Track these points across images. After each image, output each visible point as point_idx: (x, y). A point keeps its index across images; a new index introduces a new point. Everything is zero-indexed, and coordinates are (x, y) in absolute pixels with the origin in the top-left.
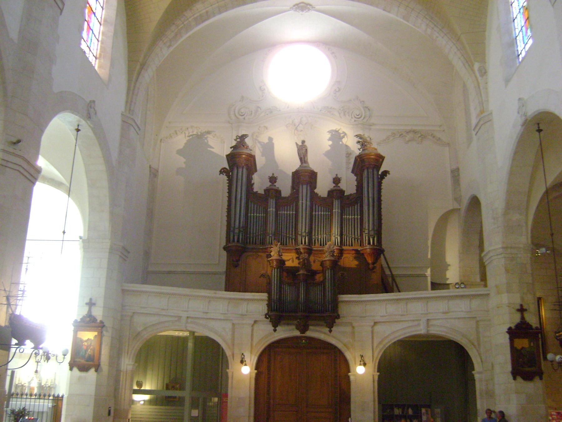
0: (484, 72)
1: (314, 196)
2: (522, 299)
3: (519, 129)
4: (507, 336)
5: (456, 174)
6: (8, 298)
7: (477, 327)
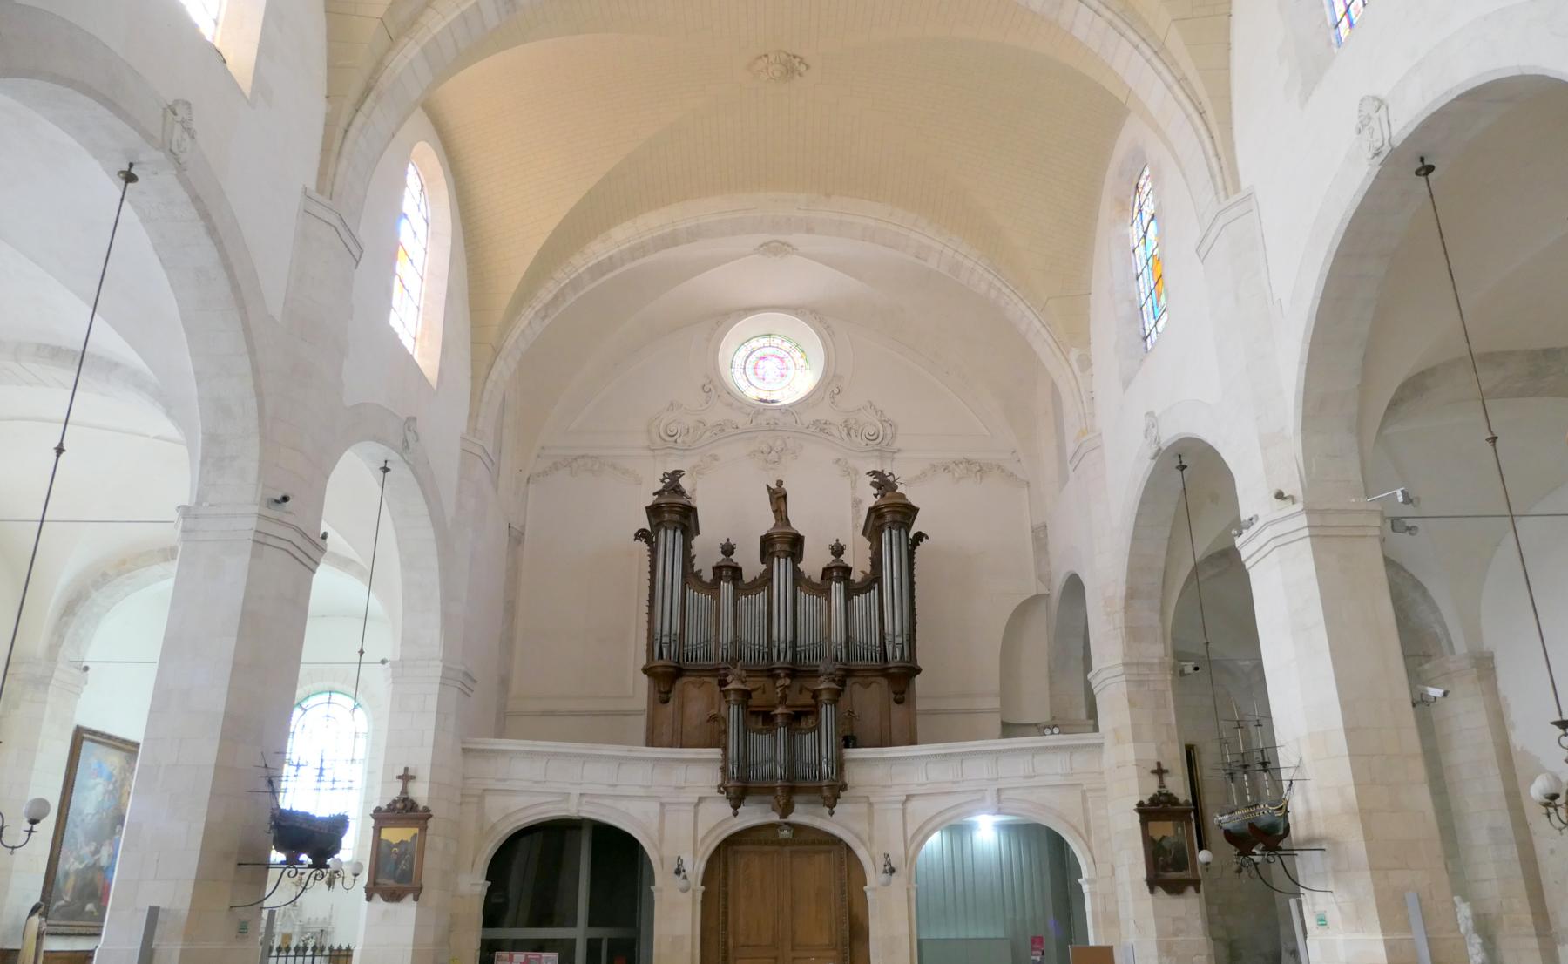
0: (1086, 363)
1: (798, 578)
2: (1159, 750)
3: (1147, 465)
4: (1137, 816)
5: (1040, 535)
6: (270, 782)
7: (1084, 800)
